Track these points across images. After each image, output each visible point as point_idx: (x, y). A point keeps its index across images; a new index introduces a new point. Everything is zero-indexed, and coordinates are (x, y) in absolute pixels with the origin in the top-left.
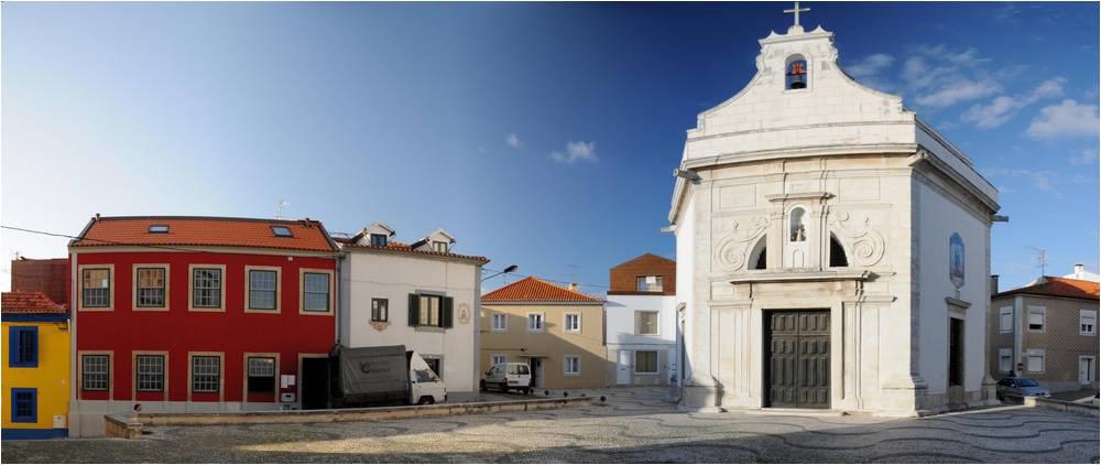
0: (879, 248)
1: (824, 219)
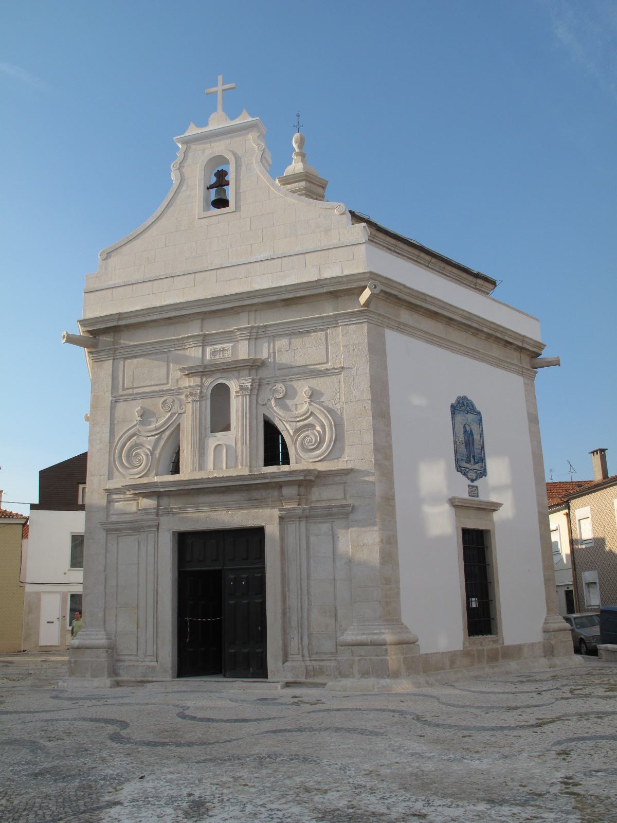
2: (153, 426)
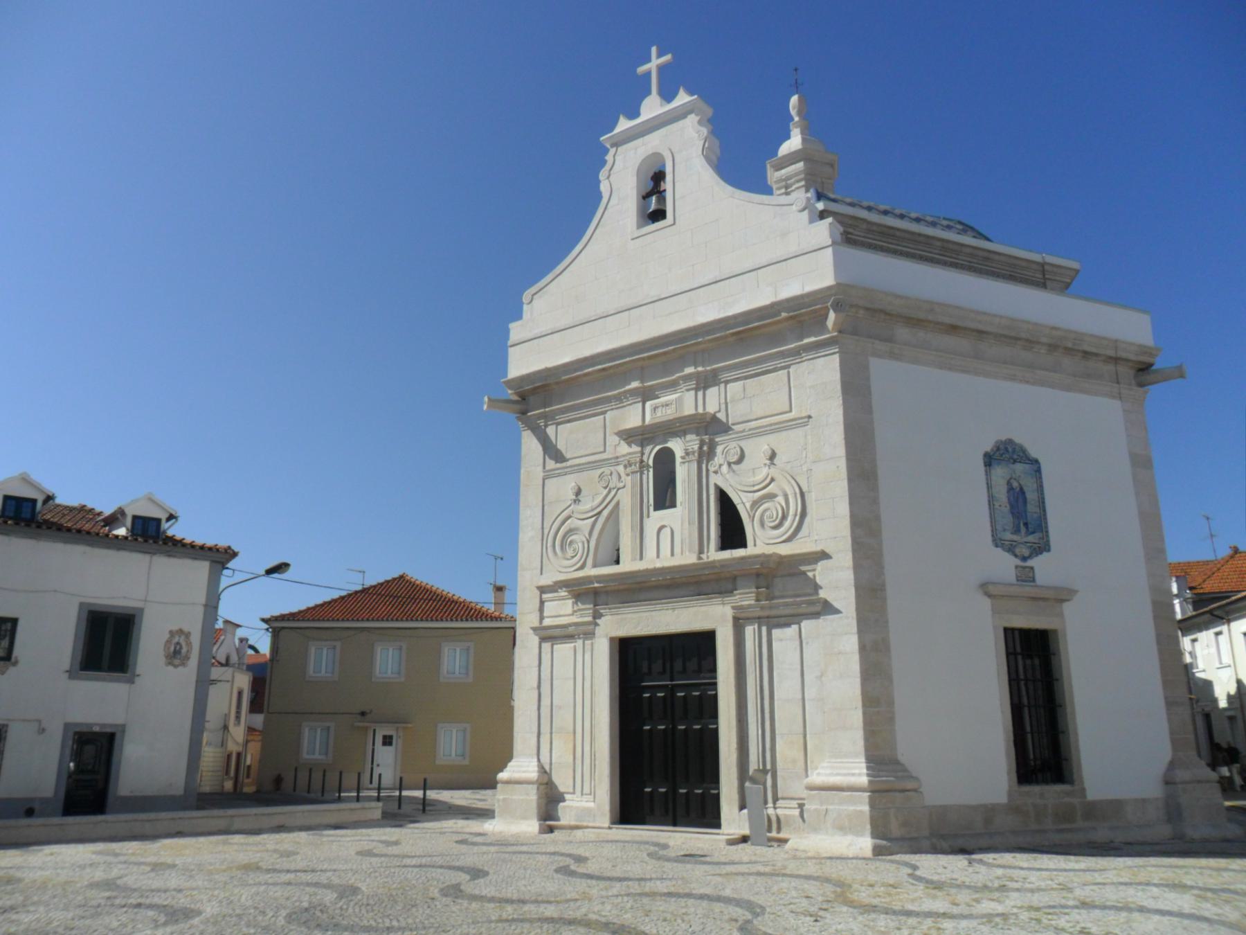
2: (588, 507)
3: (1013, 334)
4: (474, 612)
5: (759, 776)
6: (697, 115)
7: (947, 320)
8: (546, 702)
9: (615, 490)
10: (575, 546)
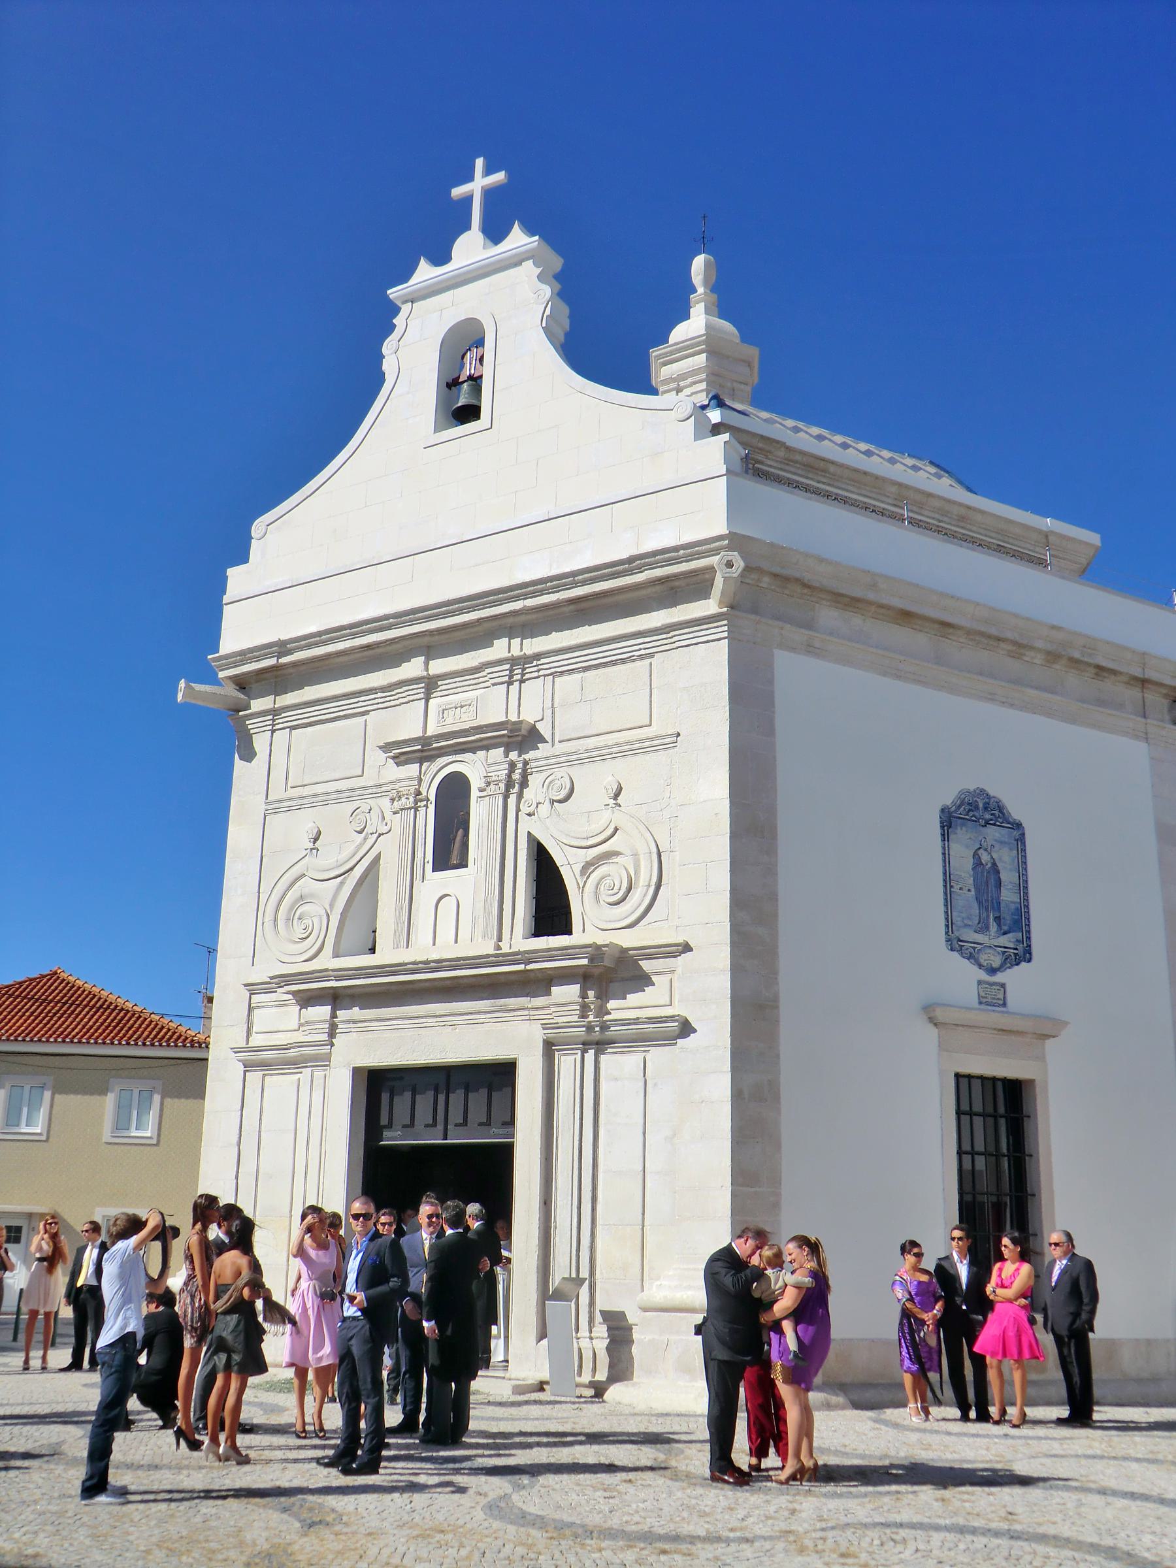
0: (646, 875)
1: (512, 800)
2: (332, 861)
3: (993, 631)
4: (166, 1034)
5: (568, 1288)
6: (536, 265)
7: (897, 603)
8: (248, 1166)
9: (375, 836)
10: (308, 922)
